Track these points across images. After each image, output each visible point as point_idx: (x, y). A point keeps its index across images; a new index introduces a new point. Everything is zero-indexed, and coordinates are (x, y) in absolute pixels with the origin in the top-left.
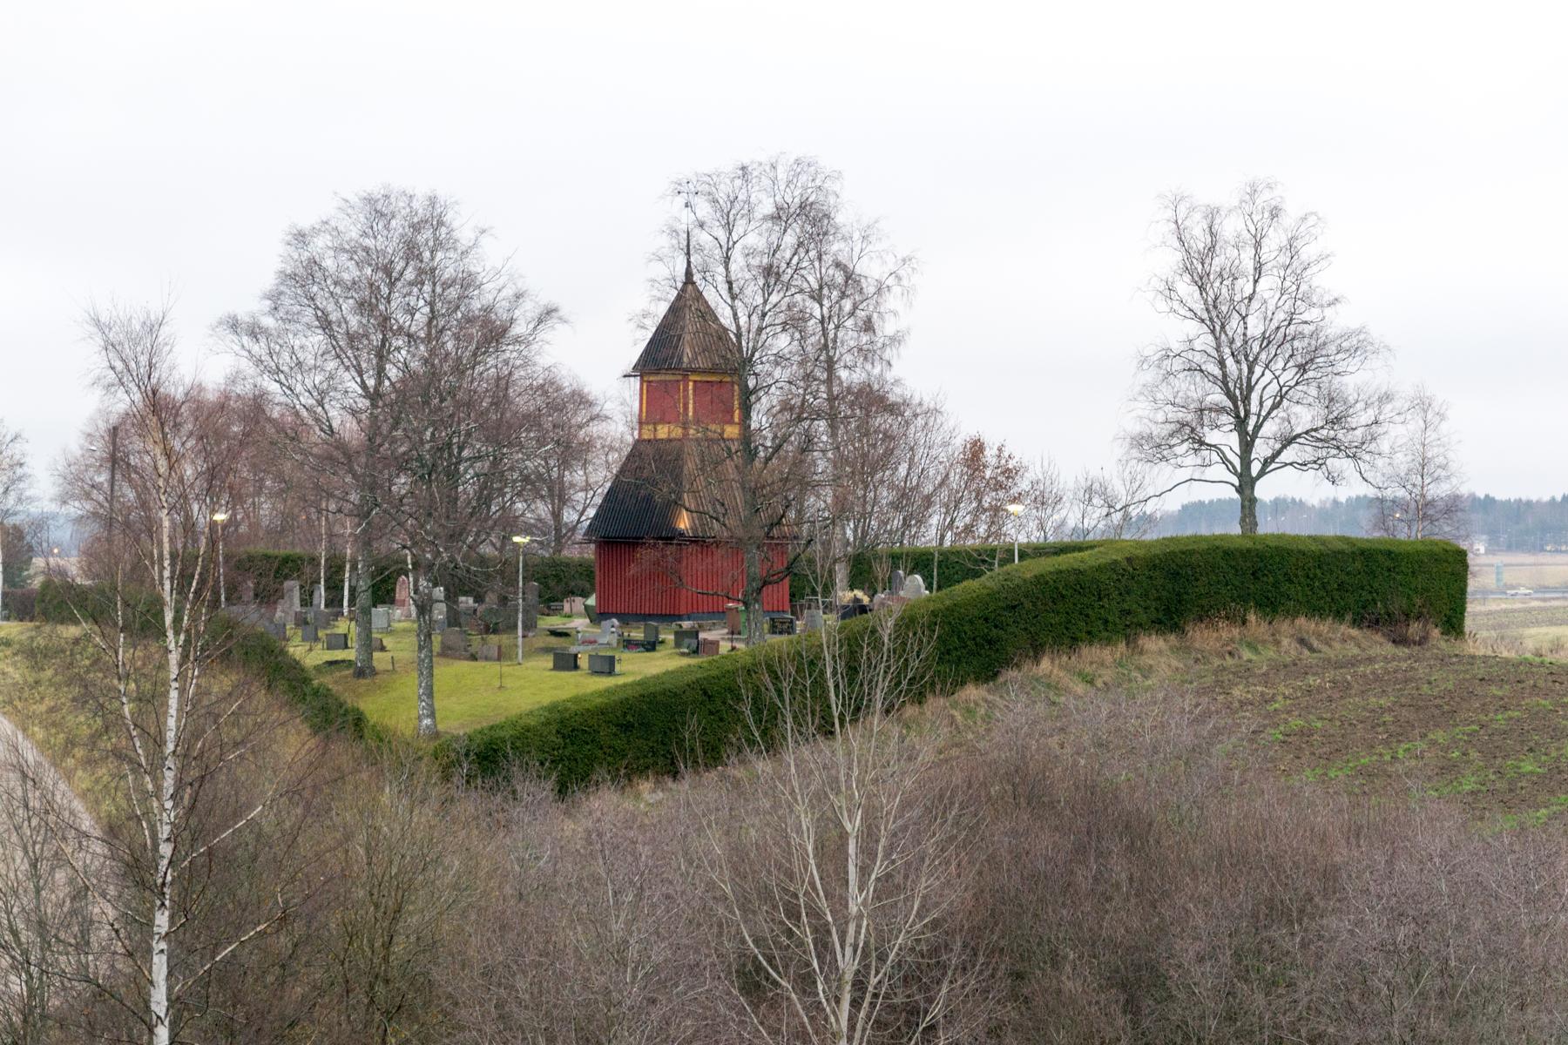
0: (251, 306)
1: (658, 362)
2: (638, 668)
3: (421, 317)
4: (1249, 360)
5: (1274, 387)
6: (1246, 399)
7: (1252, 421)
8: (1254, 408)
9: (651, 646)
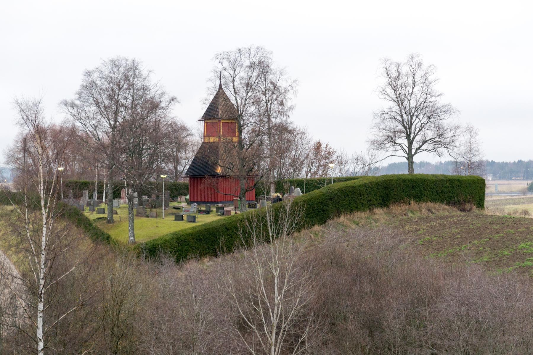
0: (72, 97)
1: (210, 115)
2: (204, 220)
5: (419, 124)
6: (410, 128)
8: (413, 131)
9: (208, 212)
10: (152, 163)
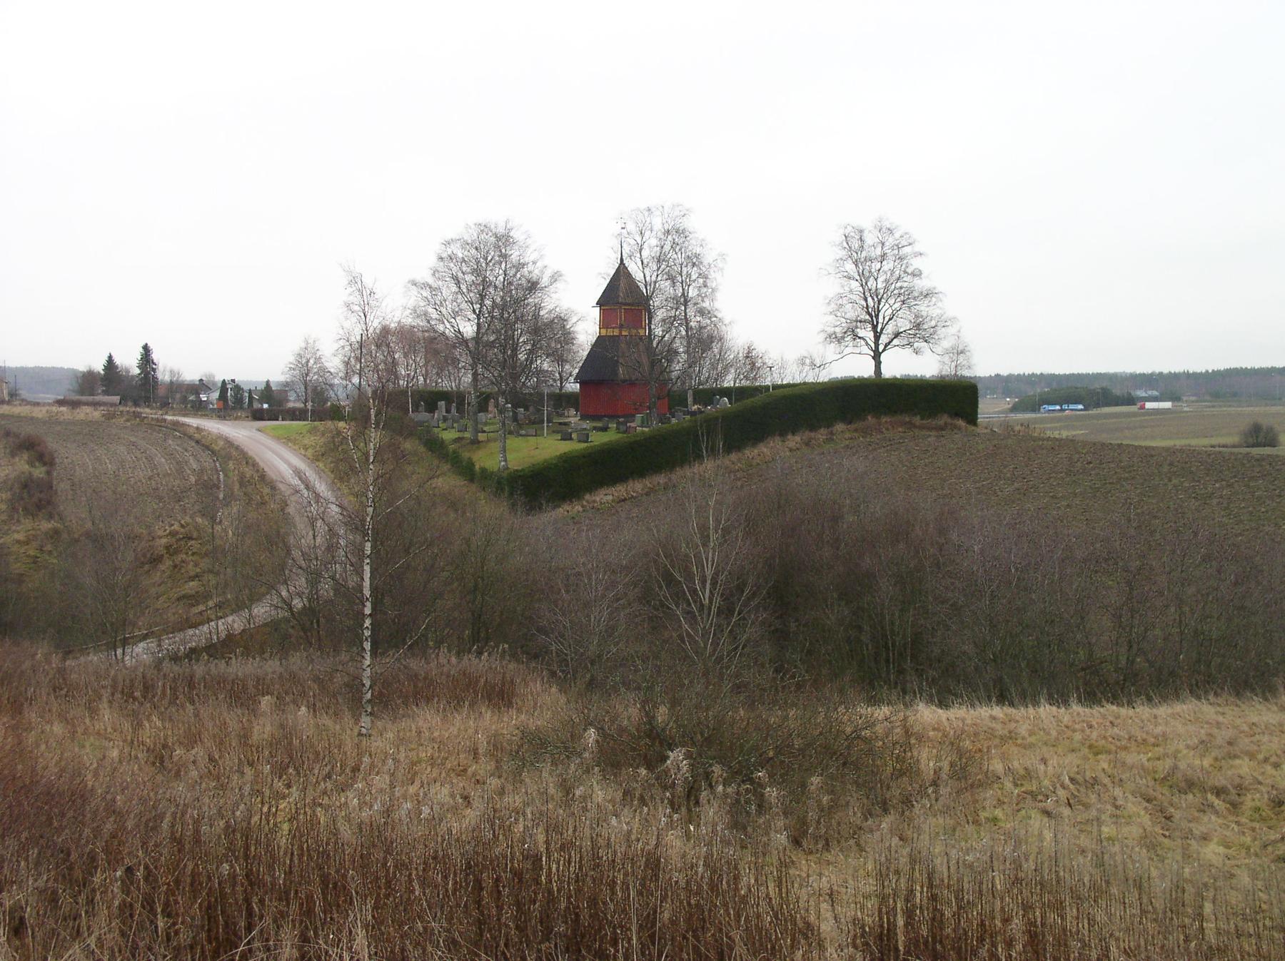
0: (425, 276)
1: (608, 301)
2: (598, 439)
3: (501, 278)
4: (880, 290)
5: (890, 311)
6: (877, 316)
7: (880, 327)
8: (881, 320)
9: (605, 429)
10: (531, 363)
